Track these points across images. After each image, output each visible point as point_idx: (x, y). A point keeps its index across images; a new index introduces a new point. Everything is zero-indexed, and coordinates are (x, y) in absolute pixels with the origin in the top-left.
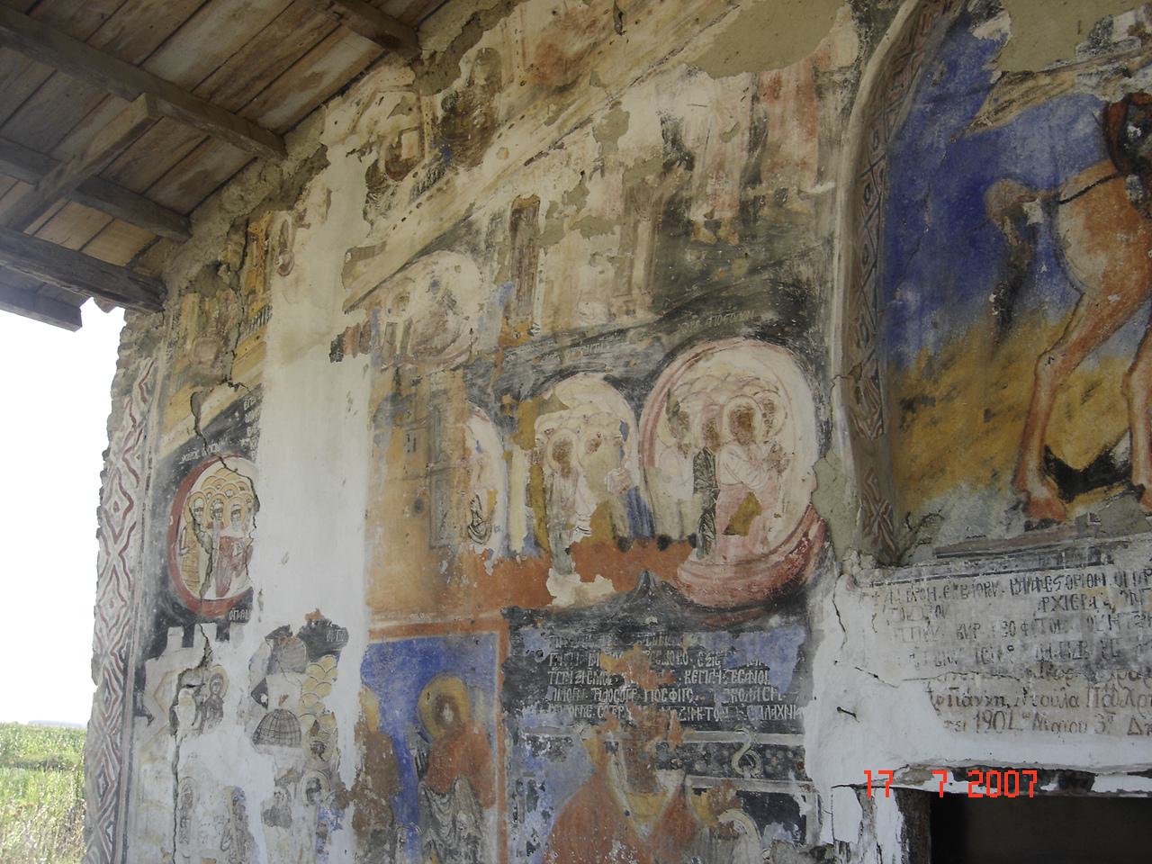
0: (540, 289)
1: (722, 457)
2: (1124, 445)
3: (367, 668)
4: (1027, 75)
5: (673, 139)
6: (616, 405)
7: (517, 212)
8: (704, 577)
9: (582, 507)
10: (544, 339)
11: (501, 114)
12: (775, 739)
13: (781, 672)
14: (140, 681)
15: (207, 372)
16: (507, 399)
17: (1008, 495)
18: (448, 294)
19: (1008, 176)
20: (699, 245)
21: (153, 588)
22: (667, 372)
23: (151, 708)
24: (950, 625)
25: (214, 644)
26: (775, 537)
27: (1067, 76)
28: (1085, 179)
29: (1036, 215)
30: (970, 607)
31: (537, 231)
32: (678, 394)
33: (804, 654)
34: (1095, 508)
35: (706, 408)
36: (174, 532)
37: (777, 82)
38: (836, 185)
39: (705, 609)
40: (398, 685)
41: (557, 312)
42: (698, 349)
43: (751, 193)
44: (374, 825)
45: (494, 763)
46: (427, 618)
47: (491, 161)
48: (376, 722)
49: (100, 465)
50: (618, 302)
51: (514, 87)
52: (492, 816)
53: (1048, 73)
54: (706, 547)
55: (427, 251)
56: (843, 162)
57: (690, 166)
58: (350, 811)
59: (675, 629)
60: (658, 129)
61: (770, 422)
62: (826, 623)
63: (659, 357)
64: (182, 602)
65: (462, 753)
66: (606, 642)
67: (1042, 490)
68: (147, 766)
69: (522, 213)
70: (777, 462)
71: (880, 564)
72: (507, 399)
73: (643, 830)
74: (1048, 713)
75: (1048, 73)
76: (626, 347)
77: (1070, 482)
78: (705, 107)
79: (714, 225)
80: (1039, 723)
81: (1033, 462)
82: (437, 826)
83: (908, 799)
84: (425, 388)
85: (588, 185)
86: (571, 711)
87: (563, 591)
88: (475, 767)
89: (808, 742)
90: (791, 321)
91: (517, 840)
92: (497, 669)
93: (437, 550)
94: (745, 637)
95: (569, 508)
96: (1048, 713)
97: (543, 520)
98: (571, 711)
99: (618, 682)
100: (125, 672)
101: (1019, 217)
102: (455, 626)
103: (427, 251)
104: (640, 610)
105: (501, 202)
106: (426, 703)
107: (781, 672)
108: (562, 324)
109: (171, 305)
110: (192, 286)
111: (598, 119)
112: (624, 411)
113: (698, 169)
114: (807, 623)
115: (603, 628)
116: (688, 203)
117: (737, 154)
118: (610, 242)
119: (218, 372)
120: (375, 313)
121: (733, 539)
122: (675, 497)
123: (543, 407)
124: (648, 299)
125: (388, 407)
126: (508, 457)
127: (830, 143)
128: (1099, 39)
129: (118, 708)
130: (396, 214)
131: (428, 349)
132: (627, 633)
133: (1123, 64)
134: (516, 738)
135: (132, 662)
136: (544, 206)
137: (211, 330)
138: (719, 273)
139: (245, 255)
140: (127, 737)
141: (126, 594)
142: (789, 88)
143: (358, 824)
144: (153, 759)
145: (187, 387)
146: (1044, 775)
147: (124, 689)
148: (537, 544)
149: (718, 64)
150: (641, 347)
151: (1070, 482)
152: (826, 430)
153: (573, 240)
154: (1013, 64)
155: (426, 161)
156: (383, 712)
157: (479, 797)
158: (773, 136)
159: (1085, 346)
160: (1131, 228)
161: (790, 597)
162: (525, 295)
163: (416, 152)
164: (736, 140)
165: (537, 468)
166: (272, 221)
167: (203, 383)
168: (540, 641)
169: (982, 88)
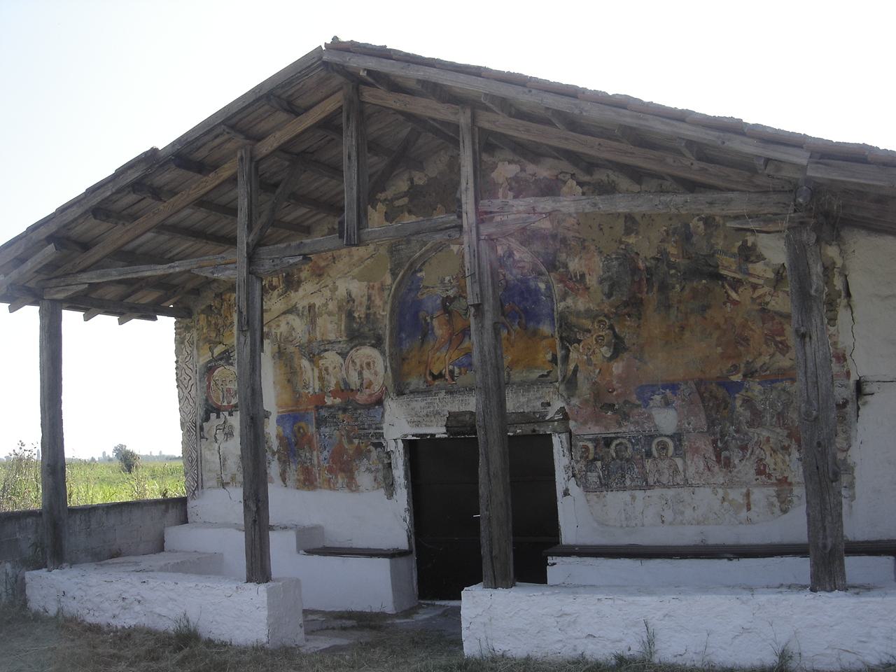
0: (318, 329)
1: (364, 372)
2: (444, 370)
3: (278, 421)
4: (427, 287)
5: (349, 294)
6: (339, 359)
7: (310, 307)
8: (361, 398)
9: (332, 383)
10: (320, 341)
11: (303, 278)
12: (378, 431)
13: (378, 417)
14: (202, 429)
15: (213, 339)
16: (311, 355)
17: (423, 379)
18: (292, 326)
19: (424, 310)
20: (357, 323)
21: (203, 403)
22: (351, 352)
23: (206, 435)
24: (410, 407)
25: (228, 417)
26: (376, 390)
27: (436, 289)
28: (439, 313)
29: (429, 320)
30: (414, 404)
31: (315, 313)
32: (354, 358)
33: (383, 414)
34: (439, 383)
35: (361, 361)
36: (209, 387)
37: (373, 286)
38: (387, 313)
39: (361, 405)
40: (287, 425)
41: (323, 335)
42: (358, 348)
43: (368, 312)
44: (283, 458)
45: (315, 441)
46: (294, 408)
47: (301, 292)
48: (282, 434)
49: (175, 365)
50: (338, 334)
51: (306, 272)
52: (315, 453)
53: (433, 287)
54: (361, 392)
55: (284, 313)
56: (388, 307)
57: (354, 303)
58: (276, 456)
59: (356, 409)
60: (346, 292)
61: (373, 365)
62: (387, 407)
63: (349, 348)
64: (214, 406)
65: (717, 218)
66: (340, 412)
67: (429, 379)
68: (208, 452)
69: (311, 307)
70: (376, 374)
71: (398, 395)
72: (311, 355)
73: (351, 452)
74: (428, 424)
75: (433, 287)
76: (341, 345)
77: (435, 377)
78: (357, 288)
79: (360, 318)
80: (426, 425)
81: (428, 372)
82: (301, 457)
83: (403, 441)
84: (287, 350)
85: (329, 303)
86: (333, 428)
87: (329, 401)
88: (310, 442)
89: (384, 431)
90: (378, 343)
91: (322, 458)
92: (314, 420)
93: (295, 392)
94: (371, 410)
95: (330, 383)
96: (428, 424)
97: (323, 385)
98: (333, 428)
99: (344, 421)
100: (195, 427)
101: (426, 320)
102: (302, 410)
103: (284, 313)
104: (347, 405)
105: (305, 303)
106: (295, 428)
107: (378, 417)
108: (324, 338)
109: (195, 316)
110: (203, 312)
111: (330, 286)
112: (341, 360)
113: (356, 303)
114: (383, 407)
115: (339, 409)
116: (354, 312)
117: (365, 299)
118: (335, 318)
119: (217, 340)
120: (270, 329)
121: (367, 390)
122: (354, 379)
123: (321, 358)
124: (345, 335)
125: (277, 355)
126: (313, 369)
127: (386, 303)
128: (442, 282)
129: (194, 437)
130: (273, 301)
131: (288, 340)
132: (345, 410)
133: (447, 288)
134: (320, 435)
135: (198, 424)
136: (317, 306)
137: (213, 327)
138: (362, 330)
139: (222, 305)
140: (199, 445)
141: (193, 405)
142: (376, 287)
143: (279, 459)
144: (209, 450)
145: (207, 344)
146: (427, 435)
147: (196, 432)
148: (322, 390)
149: (360, 278)
150: (345, 346)
151: (435, 377)
152: (386, 368)
153: (325, 316)
154: (426, 284)
155: (281, 287)
156: (284, 432)
157: (311, 449)
158: (373, 298)
159: (438, 350)
160: (446, 326)
161: (380, 402)
162: (314, 329)
163: (277, 284)
164: (364, 298)
165: (320, 372)
166: (230, 296)
167: (213, 344)
168: (324, 413)
169: (418, 289)
